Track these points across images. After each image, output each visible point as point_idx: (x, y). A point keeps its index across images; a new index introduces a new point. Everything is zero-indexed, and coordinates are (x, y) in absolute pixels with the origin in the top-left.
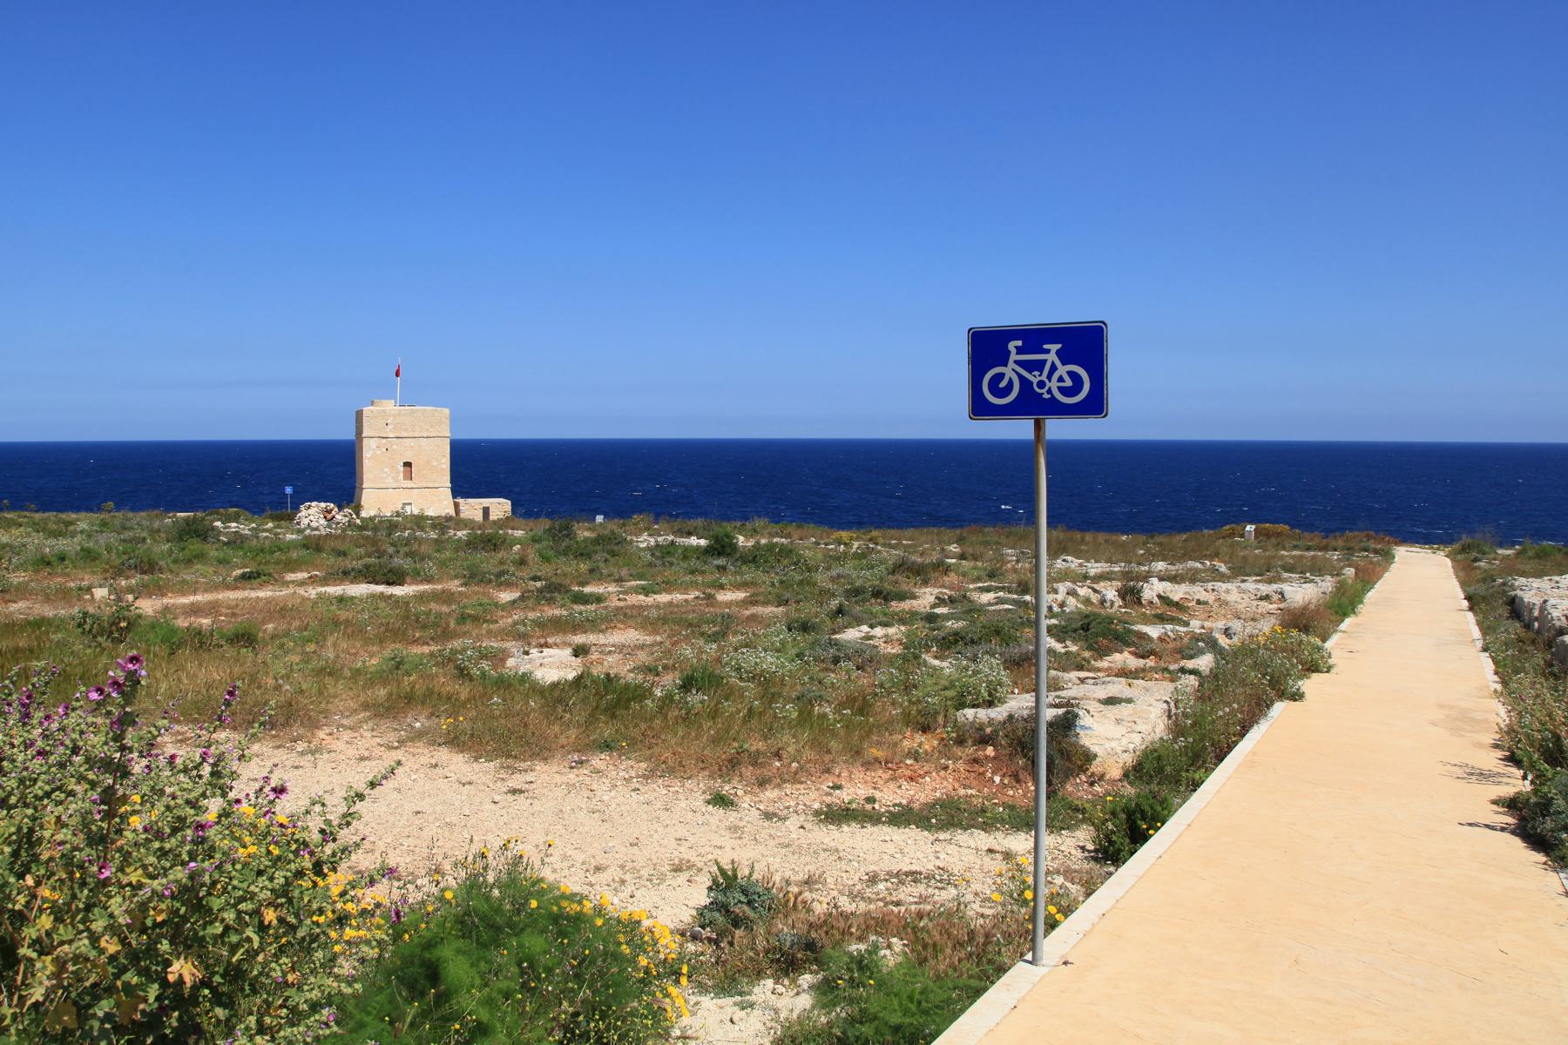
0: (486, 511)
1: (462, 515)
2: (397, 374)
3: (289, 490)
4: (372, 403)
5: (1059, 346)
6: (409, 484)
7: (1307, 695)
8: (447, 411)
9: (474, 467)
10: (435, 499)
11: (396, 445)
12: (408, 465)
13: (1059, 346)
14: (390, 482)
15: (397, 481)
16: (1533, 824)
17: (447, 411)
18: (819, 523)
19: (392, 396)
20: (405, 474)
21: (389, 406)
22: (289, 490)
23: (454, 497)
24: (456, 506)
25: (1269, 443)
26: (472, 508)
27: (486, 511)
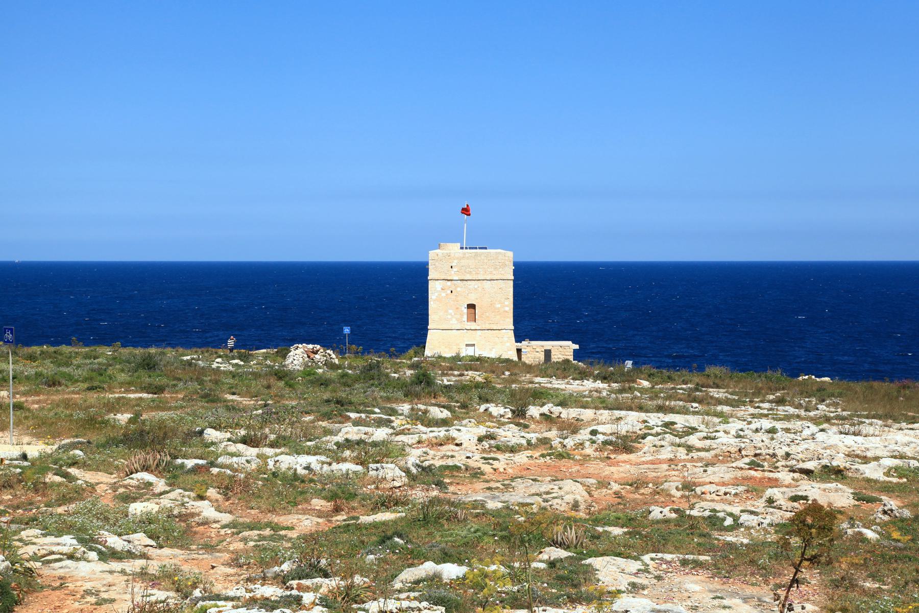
0: (548, 353)
1: (524, 358)
3: (347, 330)
4: (439, 247)
5: (577, 347)
6: (473, 325)
8: (510, 254)
9: (546, 299)
10: (497, 340)
11: (460, 288)
12: (471, 307)
13: (577, 347)
14: (454, 323)
17: (510, 254)
18: (846, 371)
20: (470, 311)
21: (454, 248)
22: (347, 330)
24: (519, 351)
26: (534, 351)
27: (548, 353)
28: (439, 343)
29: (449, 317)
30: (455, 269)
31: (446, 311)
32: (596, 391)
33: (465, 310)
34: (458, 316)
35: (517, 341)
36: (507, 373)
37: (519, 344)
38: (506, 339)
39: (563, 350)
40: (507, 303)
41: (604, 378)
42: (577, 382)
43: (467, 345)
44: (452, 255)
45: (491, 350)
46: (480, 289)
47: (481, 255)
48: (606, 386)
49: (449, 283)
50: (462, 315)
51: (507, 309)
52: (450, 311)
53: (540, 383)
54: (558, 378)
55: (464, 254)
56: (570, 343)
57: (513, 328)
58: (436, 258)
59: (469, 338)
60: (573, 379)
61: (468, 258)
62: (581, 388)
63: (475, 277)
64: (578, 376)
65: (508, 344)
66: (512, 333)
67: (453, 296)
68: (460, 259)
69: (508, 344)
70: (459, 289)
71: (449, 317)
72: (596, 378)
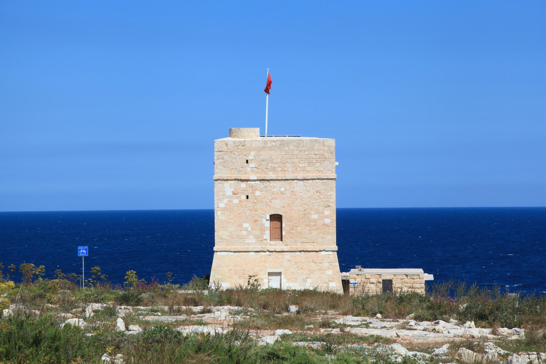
2: (267, 91)
3: (83, 251)
4: (230, 133)
5: (431, 277)
6: (278, 245)
7: (279, 212)
8: (331, 142)
10: (323, 272)
11: (259, 191)
12: (276, 218)
13: (431, 277)
14: (252, 243)
15: (261, 241)
16: (281, 216)
17: (331, 142)
19: (254, 121)
21: (251, 135)
22: (83, 251)
23: (344, 268)
24: (346, 283)
25: (538, 208)
26: (368, 279)
27: (387, 284)
28: (226, 272)
29: (244, 233)
30: (252, 165)
31: (240, 225)
32: (470, 346)
33: (268, 224)
34: (258, 232)
35: (342, 271)
36: (293, 308)
37: (344, 274)
38: (326, 265)
39: (412, 279)
40: (327, 213)
41: (481, 318)
42: (425, 324)
43: (270, 274)
44: (248, 145)
45: (304, 281)
46: (288, 194)
47: (289, 143)
48: (486, 332)
49: (243, 185)
50: (262, 230)
51: (327, 221)
52: (246, 225)
53: (343, 326)
54: (385, 317)
55: (265, 142)
56: (420, 271)
57: (336, 248)
58: (225, 148)
59: (273, 263)
60: (416, 318)
61: (270, 149)
62: (432, 337)
63: (281, 176)
64: (427, 313)
65: (330, 272)
66: (334, 257)
67: (249, 203)
68: (258, 150)
69: (330, 272)
70: (258, 193)
71: (244, 233)
72: (462, 318)
